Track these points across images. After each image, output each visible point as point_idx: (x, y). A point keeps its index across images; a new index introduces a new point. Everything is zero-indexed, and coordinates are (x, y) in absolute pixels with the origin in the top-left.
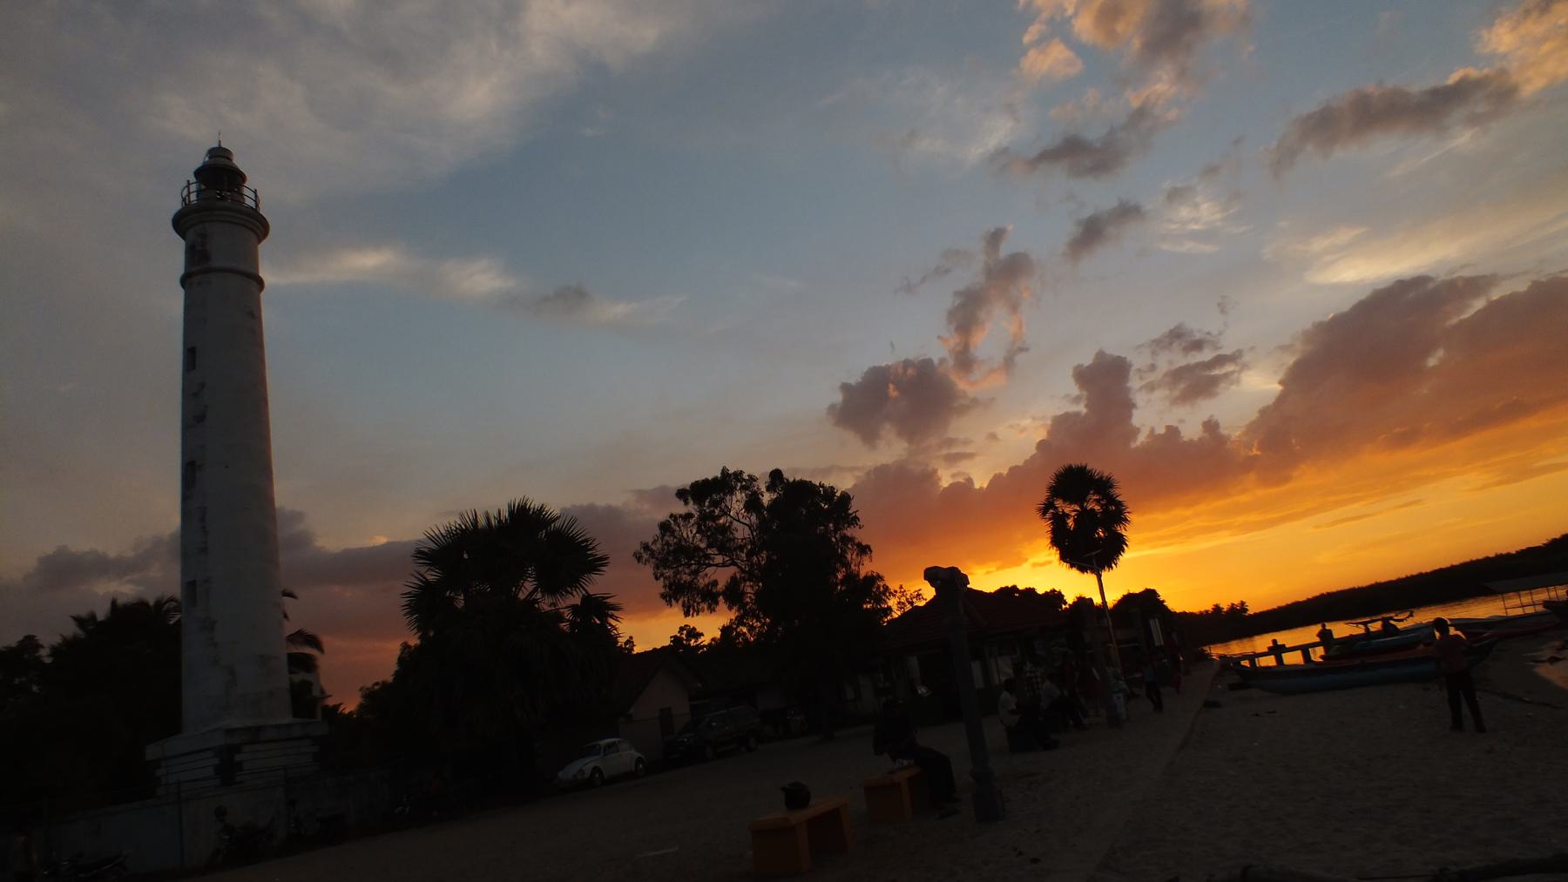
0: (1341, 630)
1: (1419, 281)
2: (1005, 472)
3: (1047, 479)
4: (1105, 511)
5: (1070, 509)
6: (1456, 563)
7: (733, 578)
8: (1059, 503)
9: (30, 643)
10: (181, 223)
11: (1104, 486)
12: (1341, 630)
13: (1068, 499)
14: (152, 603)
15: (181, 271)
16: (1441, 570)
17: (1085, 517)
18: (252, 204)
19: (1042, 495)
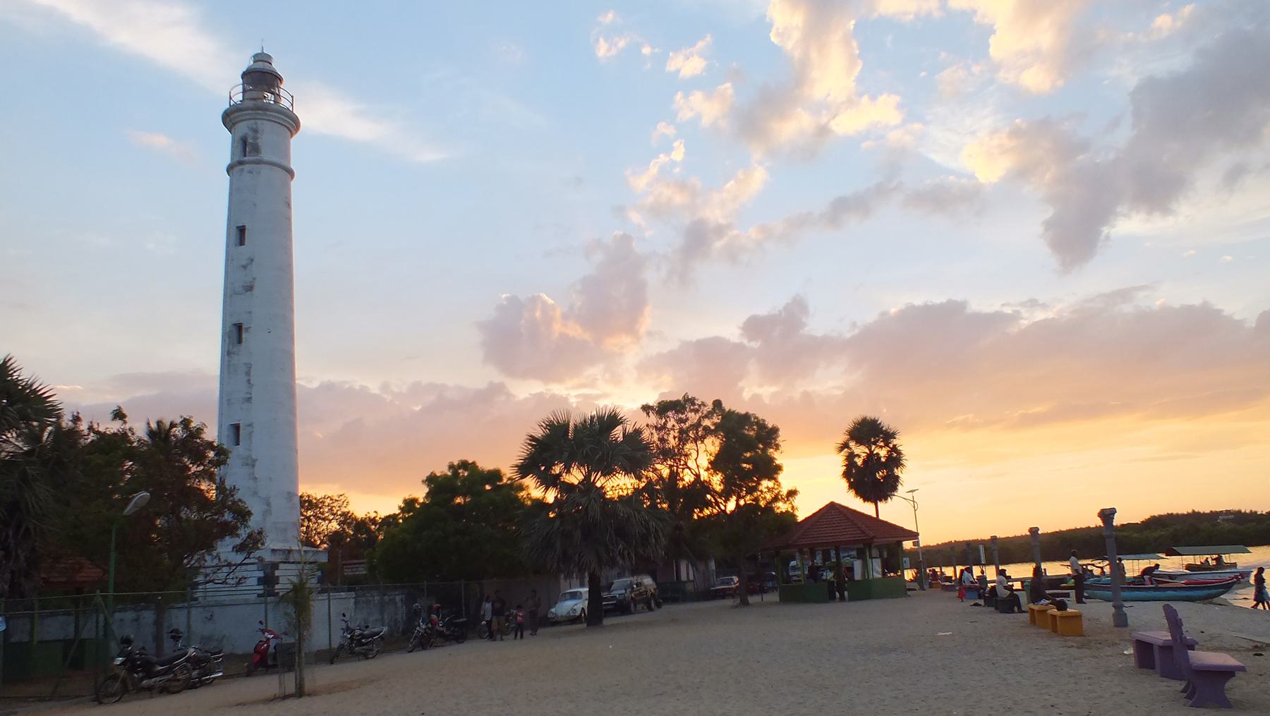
0: (1054, 569)
1: (928, 309)
2: (139, 429)
3: (848, 424)
4: (889, 458)
5: (861, 451)
6: (1064, 529)
7: (568, 472)
8: (852, 444)
9: (777, 447)
10: (230, 118)
11: (888, 436)
12: (1054, 569)
13: (860, 442)
14: (770, 426)
15: (228, 161)
16: (1061, 532)
17: (871, 459)
18: (287, 105)
19: (843, 438)
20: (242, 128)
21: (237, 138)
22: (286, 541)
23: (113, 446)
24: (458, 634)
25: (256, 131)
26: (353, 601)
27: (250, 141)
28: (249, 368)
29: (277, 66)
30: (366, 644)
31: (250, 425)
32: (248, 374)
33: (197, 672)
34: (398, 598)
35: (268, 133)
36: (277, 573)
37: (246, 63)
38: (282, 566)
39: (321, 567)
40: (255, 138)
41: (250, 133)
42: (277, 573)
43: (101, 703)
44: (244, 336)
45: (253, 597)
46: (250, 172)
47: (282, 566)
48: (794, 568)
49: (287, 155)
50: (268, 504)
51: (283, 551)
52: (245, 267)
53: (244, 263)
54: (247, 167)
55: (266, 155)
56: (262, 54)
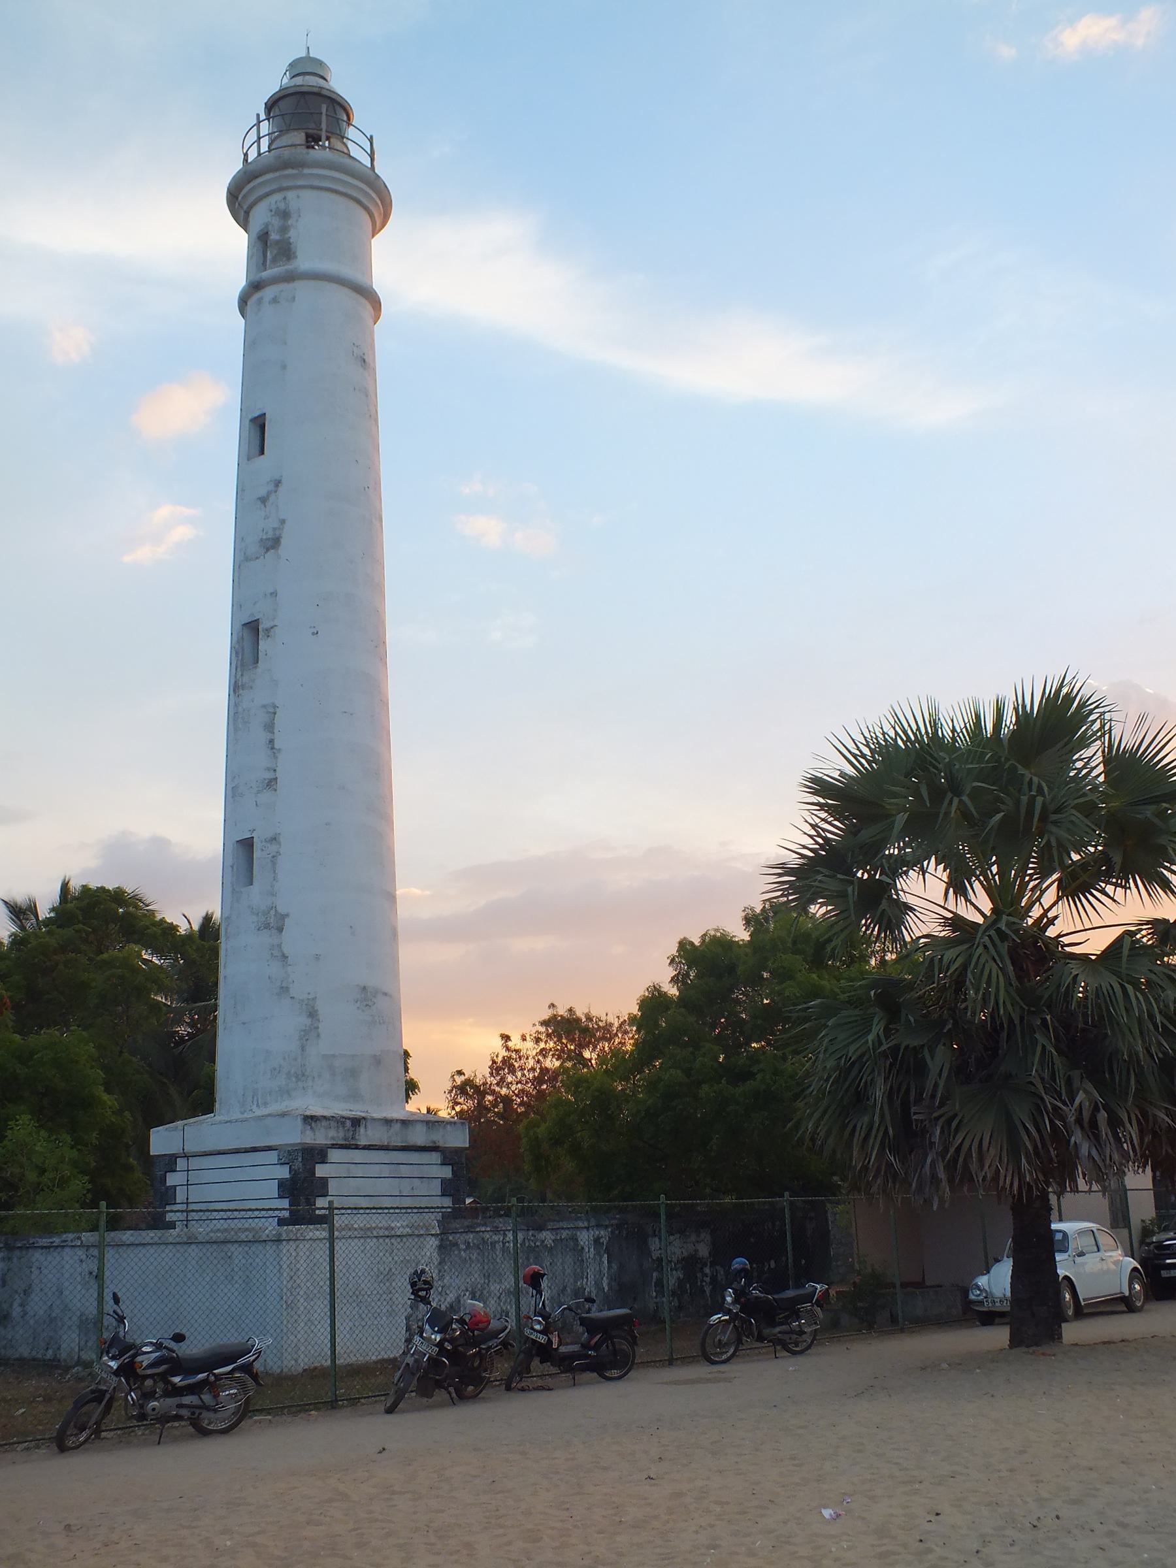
15: (239, 279)
20: (261, 215)
21: (254, 235)
22: (355, 1096)
23: (865, 777)
24: (769, 1326)
25: (285, 215)
26: (434, 1242)
27: (274, 236)
28: (272, 712)
29: (339, 83)
30: (178, 1391)
31: (274, 839)
32: (270, 727)
33: (191, 1391)
34: (585, 1238)
35: (314, 219)
36: (321, 1171)
37: (274, 81)
38: (334, 1155)
39: (450, 1156)
40: (284, 229)
41: (276, 222)
42: (321, 1171)
43: (63, 1449)
44: (263, 645)
45: (270, 1227)
46: (275, 300)
47: (334, 1155)
48: (539, 1323)
49: (363, 258)
50: (313, 1014)
51: (340, 1121)
52: (263, 500)
53: (263, 492)
54: (268, 293)
55: (304, 262)
56: (308, 59)
